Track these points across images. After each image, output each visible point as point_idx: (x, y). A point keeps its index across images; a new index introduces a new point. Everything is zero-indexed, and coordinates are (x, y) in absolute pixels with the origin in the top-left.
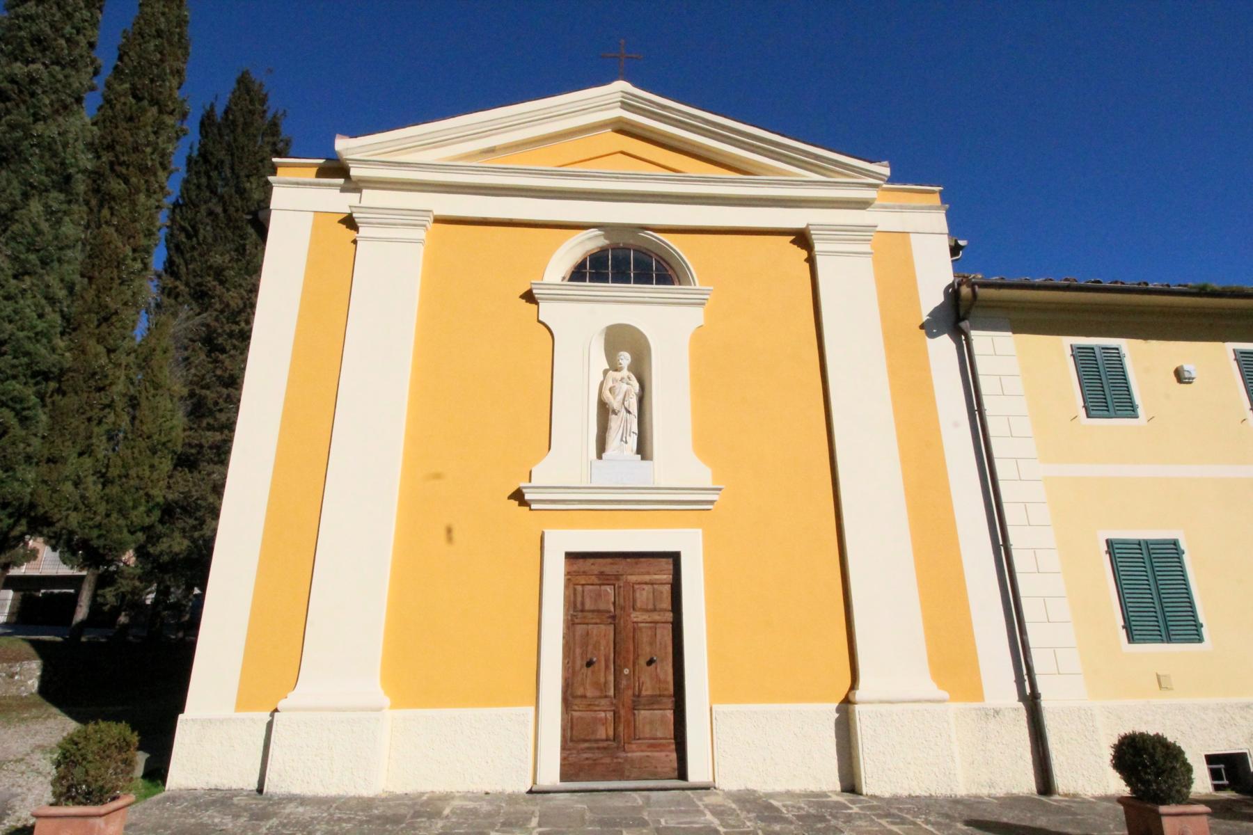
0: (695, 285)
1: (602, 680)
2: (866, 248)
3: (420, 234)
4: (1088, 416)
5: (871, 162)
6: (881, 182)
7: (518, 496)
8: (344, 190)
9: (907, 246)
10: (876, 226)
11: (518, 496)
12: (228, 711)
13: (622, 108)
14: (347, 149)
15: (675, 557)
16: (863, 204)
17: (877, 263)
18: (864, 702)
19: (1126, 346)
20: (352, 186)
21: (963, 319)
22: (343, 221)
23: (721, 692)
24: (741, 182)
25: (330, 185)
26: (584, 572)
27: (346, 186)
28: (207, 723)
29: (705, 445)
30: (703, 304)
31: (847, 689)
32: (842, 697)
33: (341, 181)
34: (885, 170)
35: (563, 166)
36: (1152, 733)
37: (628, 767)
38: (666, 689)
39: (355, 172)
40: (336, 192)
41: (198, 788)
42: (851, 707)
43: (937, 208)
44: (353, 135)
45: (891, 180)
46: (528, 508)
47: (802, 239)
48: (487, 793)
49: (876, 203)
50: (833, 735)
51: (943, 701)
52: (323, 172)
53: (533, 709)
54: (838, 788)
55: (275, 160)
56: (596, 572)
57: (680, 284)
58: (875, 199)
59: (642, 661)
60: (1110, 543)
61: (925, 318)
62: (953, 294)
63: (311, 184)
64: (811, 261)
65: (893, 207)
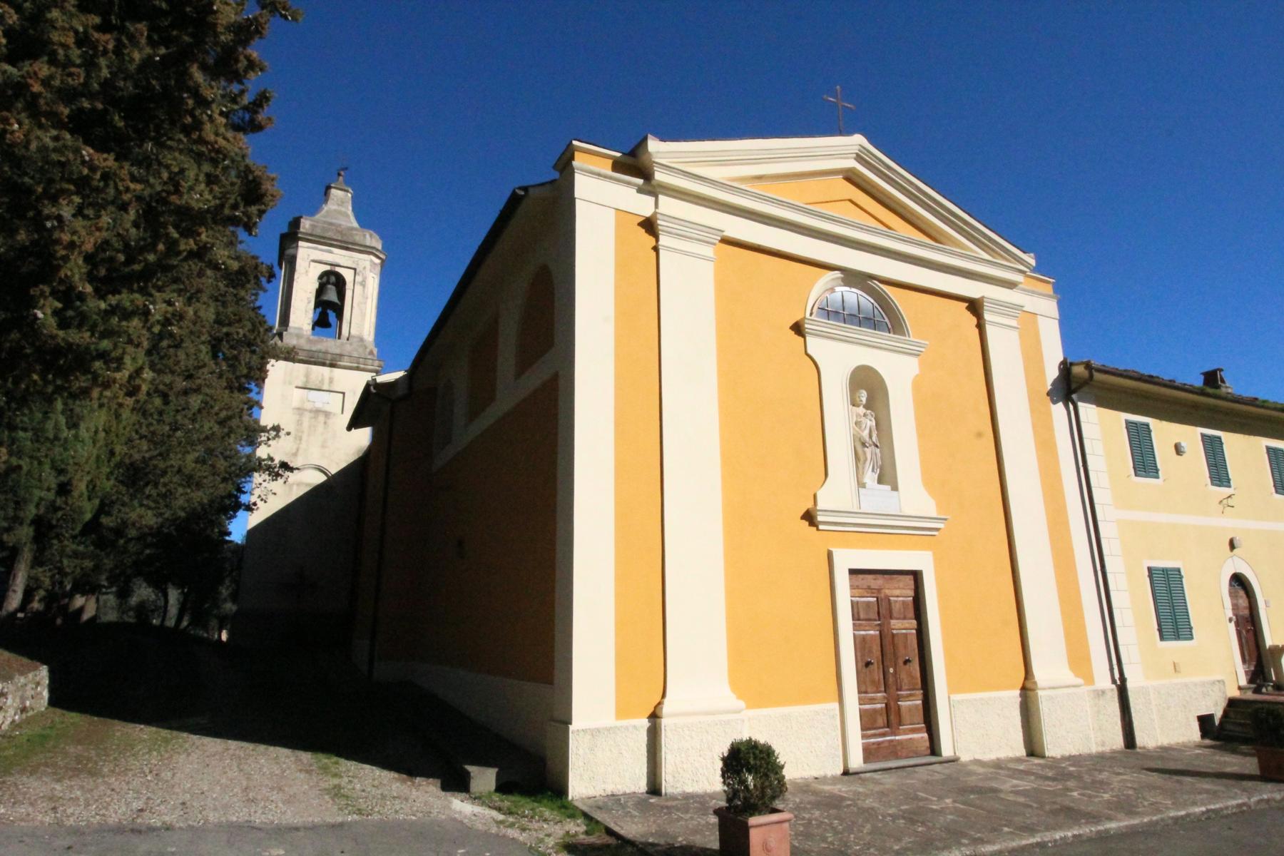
0: (909, 337)
1: (877, 678)
2: (1014, 323)
3: (708, 251)
4: (1136, 475)
5: (1024, 252)
6: (1027, 270)
7: (809, 517)
8: (640, 190)
9: (1035, 323)
10: (723, 231)
11: (809, 517)
12: (609, 720)
13: (855, 159)
14: (658, 152)
15: (916, 576)
16: (1011, 285)
17: (1021, 336)
18: (1044, 689)
19: (1153, 423)
20: (650, 188)
21: (1074, 392)
22: (642, 224)
23: (953, 688)
24: (933, 248)
25: (629, 183)
26: (857, 586)
27: (644, 187)
28: (595, 733)
29: (931, 481)
30: (918, 355)
31: (1023, 679)
32: (1020, 685)
33: (640, 181)
34: (1033, 262)
35: (810, 204)
36: (762, 741)
37: (899, 748)
38: (917, 684)
39: (660, 176)
40: (632, 191)
41: (598, 795)
42: (658, 720)
43: (1049, 296)
44: (663, 139)
45: (1035, 270)
46: (815, 528)
47: (975, 307)
48: (816, 778)
49: (1020, 286)
50: (1019, 714)
51: (739, 711)
52: (618, 166)
53: (836, 705)
54: (1025, 754)
55: (575, 143)
56: (865, 587)
57: (894, 334)
58: (1021, 283)
59: (901, 662)
60: (1150, 569)
61: (1049, 387)
62: (1065, 368)
63: (606, 177)
64: (981, 327)
65: (1028, 291)
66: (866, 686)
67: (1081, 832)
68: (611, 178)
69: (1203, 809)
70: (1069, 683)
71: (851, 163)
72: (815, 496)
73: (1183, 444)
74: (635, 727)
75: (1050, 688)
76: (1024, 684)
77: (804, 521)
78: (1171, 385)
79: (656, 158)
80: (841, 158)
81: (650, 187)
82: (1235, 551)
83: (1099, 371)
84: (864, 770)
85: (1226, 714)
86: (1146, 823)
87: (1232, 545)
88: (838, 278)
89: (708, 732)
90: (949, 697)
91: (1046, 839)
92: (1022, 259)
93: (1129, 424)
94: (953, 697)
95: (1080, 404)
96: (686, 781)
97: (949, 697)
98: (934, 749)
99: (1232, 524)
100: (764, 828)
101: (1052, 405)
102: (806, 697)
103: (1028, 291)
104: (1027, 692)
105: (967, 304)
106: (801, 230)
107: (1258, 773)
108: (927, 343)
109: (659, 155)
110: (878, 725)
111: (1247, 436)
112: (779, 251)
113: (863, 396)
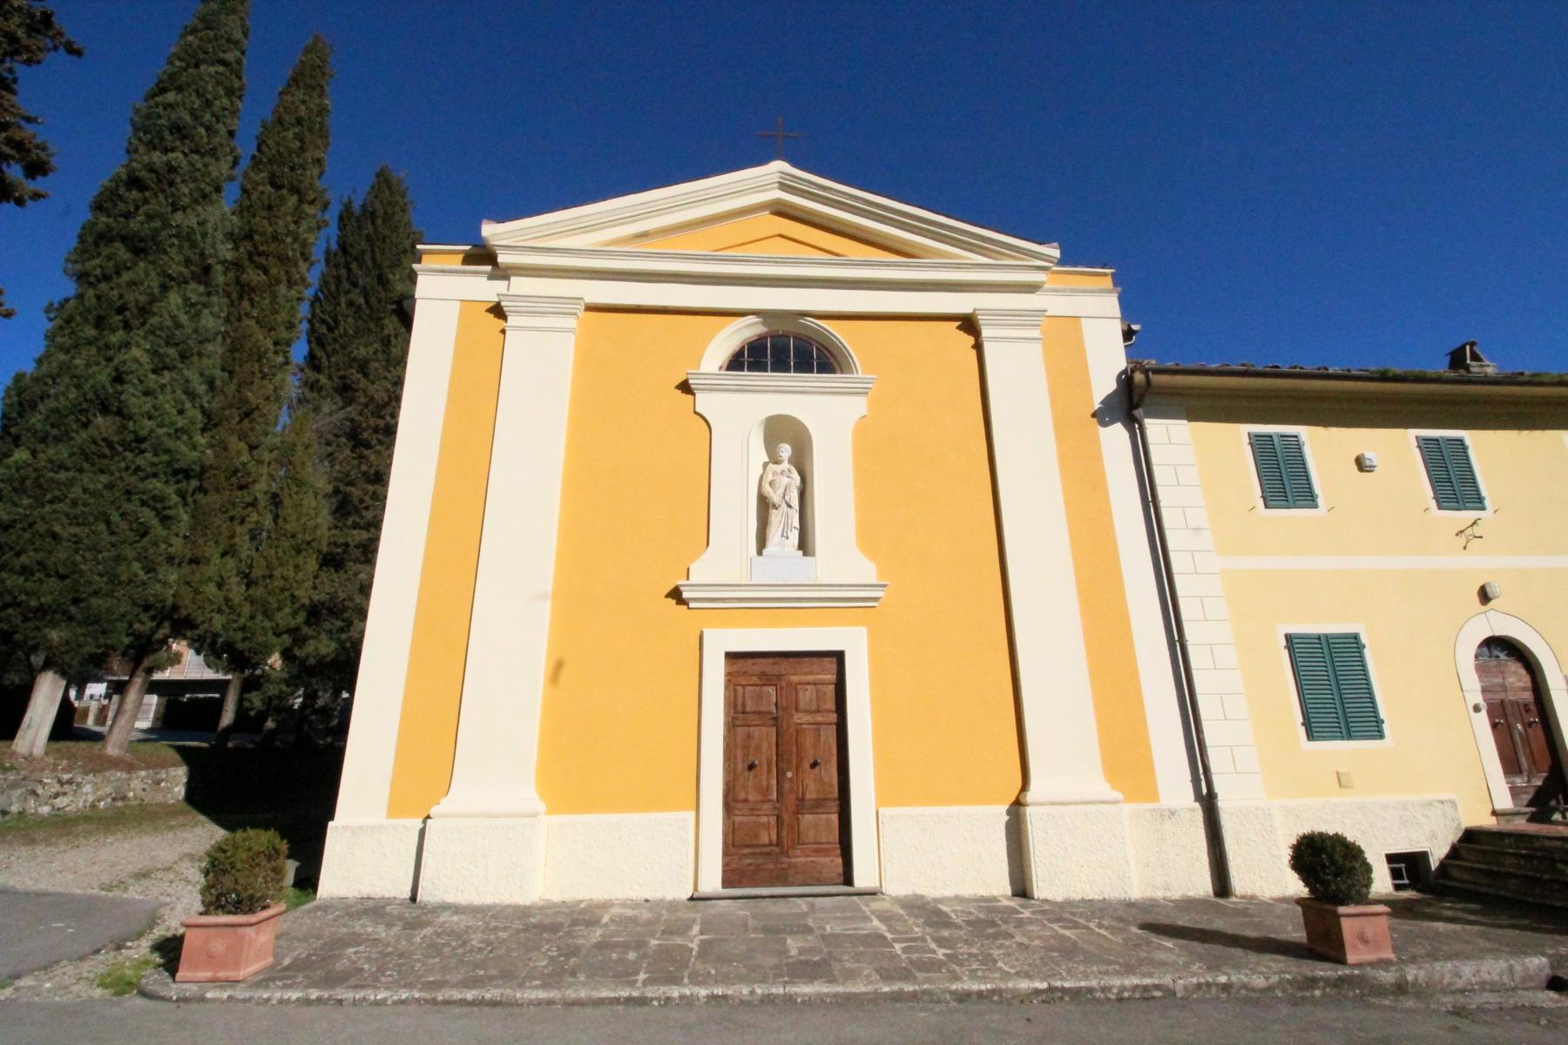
2: (1036, 333)
3: (571, 322)
4: (1266, 506)
7: (676, 595)
8: (491, 277)
9: (1077, 330)
11: (676, 595)
12: (379, 816)
13: (779, 189)
14: (494, 235)
16: (1032, 288)
21: (1137, 406)
22: (490, 310)
23: (888, 795)
24: (907, 266)
25: (477, 273)
29: (869, 539)
30: (867, 393)
31: (1018, 791)
32: (1013, 799)
33: (488, 268)
34: (1056, 253)
37: (791, 872)
39: (503, 258)
44: (501, 218)
45: (1061, 262)
46: (685, 607)
47: (969, 324)
49: (1046, 286)
52: (469, 259)
53: (693, 813)
55: (419, 247)
58: (1044, 283)
60: (1288, 638)
61: (1097, 406)
62: (1126, 381)
64: (978, 347)
66: (747, 793)
67: (730, 992)
68: (465, 272)
69: (1044, 985)
70: (1104, 798)
72: (688, 570)
73: (1367, 455)
76: (1018, 798)
77: (670, 600)
78: (1534, 381)
81: (502, 273)
82: (1492, 604)
83: (1158, 371)
84: (718, 896)
85: (1455, 852)
86: (885, 993)
87: (1484, 596)
88: (756, 323)
90: (877, 812)
91: (650, 995)
93: (1426, 445)
94: (883, 811)
97: (877, 812)
98: (848, 880)
99: (1481, 564)
100: (208, 930)
101: (1100, 428)
102: (685, 808)
107: (1300, 935)
108: (875, 376)
109: (496, 237)
110: (761, 842)
111: (1526, 433)
112: (638, 306)
113: (786, 451)
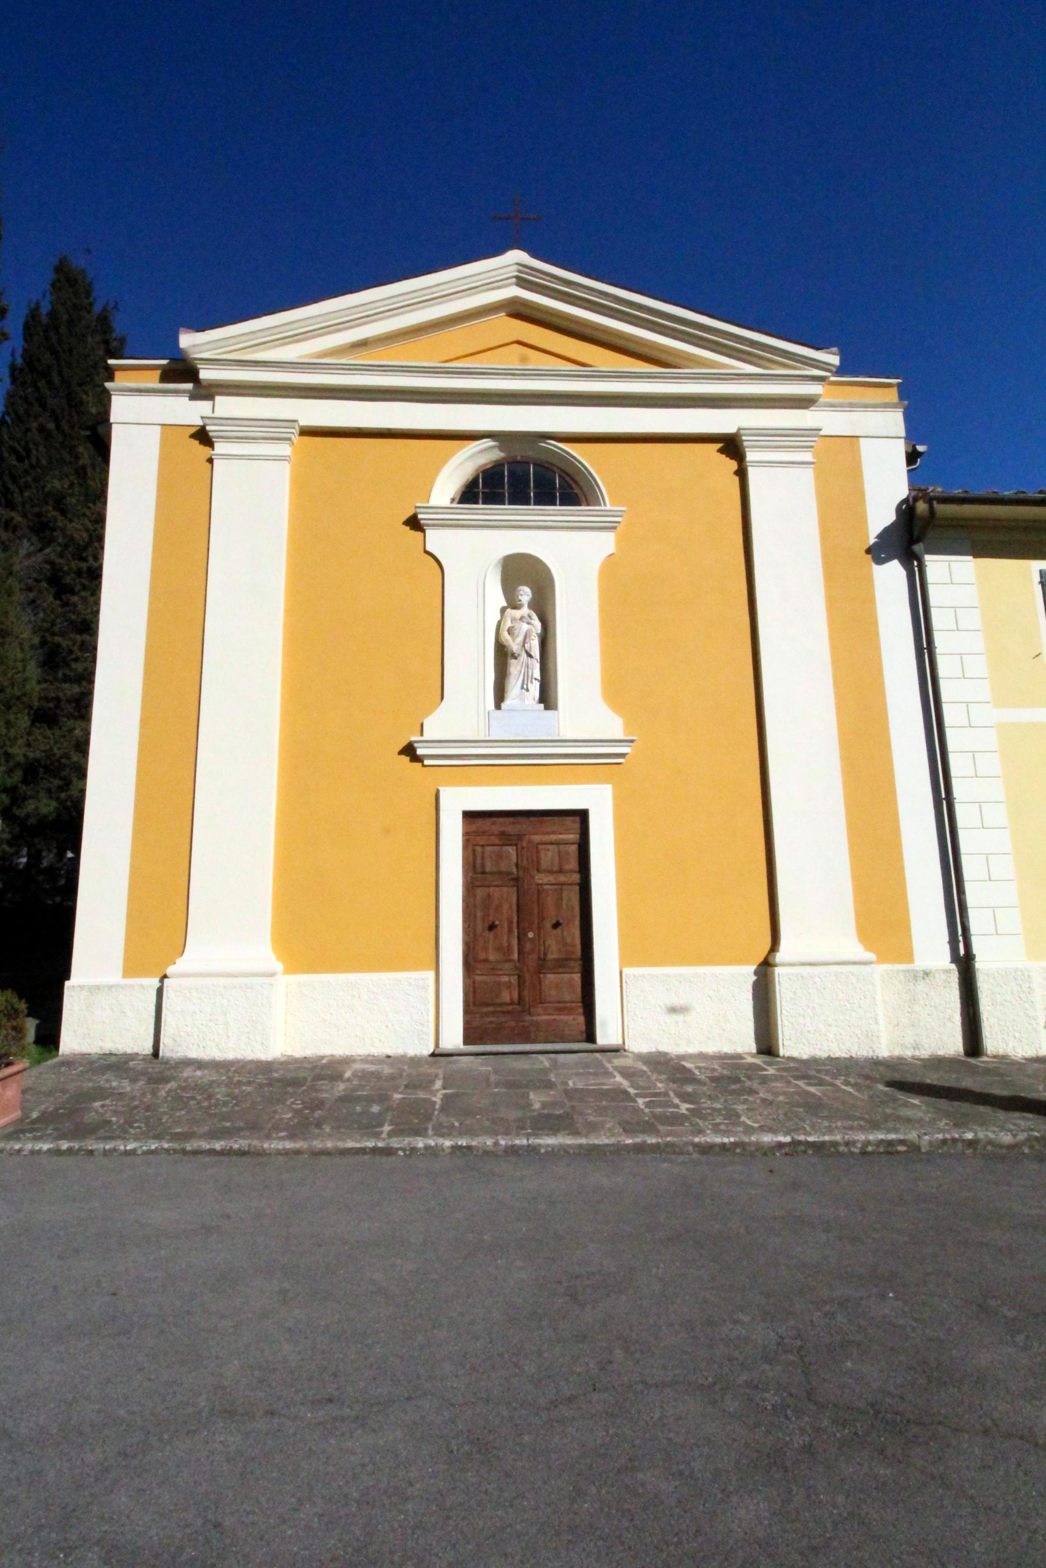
0: (605, 505)
1: (505, 944)
2: (807, 456)
3: (285, 449)
5: (817, 349)
8: (194, 397)
10: (820, 430)
11: (409, 751)
12: (114, 976)
14: (194, 346)
20: (203, 392)
21: (918, 540)
25: (177, 392)
28: (95, 989)
30: (615, 528)
32: (761, 959)
33: (189, 386)
34: (835, 360)
35: (447, 361)
37: (533, 1029)
39: (204, 374)
45: (840, 371)
46: (420, 764)
55: (111, 362)
59: (548, 925)
61: (872, 540)
62: (906, 511)
64: (742, 474)
70: (857, 959)
71: (515, 292)
74: (141, 986)
75: (803, 964)
79: (194, 353)
80: (489, 290)
81: (205, 392)
89: (222, 995)
92: (814, 360)
95: (927, 557)
96: (191, 1046)
103: (841, 406)
104: (765, 969)
105: (719, 446)
106: (424, 397)
109: (196, 349)
113: (525, 594)
